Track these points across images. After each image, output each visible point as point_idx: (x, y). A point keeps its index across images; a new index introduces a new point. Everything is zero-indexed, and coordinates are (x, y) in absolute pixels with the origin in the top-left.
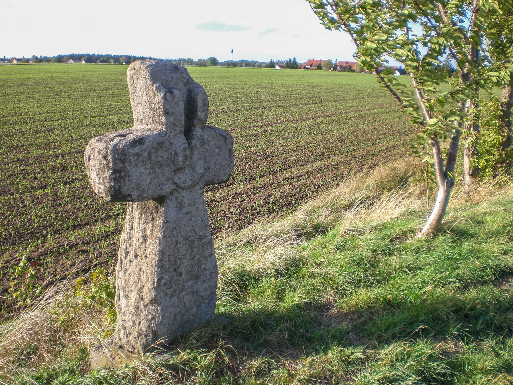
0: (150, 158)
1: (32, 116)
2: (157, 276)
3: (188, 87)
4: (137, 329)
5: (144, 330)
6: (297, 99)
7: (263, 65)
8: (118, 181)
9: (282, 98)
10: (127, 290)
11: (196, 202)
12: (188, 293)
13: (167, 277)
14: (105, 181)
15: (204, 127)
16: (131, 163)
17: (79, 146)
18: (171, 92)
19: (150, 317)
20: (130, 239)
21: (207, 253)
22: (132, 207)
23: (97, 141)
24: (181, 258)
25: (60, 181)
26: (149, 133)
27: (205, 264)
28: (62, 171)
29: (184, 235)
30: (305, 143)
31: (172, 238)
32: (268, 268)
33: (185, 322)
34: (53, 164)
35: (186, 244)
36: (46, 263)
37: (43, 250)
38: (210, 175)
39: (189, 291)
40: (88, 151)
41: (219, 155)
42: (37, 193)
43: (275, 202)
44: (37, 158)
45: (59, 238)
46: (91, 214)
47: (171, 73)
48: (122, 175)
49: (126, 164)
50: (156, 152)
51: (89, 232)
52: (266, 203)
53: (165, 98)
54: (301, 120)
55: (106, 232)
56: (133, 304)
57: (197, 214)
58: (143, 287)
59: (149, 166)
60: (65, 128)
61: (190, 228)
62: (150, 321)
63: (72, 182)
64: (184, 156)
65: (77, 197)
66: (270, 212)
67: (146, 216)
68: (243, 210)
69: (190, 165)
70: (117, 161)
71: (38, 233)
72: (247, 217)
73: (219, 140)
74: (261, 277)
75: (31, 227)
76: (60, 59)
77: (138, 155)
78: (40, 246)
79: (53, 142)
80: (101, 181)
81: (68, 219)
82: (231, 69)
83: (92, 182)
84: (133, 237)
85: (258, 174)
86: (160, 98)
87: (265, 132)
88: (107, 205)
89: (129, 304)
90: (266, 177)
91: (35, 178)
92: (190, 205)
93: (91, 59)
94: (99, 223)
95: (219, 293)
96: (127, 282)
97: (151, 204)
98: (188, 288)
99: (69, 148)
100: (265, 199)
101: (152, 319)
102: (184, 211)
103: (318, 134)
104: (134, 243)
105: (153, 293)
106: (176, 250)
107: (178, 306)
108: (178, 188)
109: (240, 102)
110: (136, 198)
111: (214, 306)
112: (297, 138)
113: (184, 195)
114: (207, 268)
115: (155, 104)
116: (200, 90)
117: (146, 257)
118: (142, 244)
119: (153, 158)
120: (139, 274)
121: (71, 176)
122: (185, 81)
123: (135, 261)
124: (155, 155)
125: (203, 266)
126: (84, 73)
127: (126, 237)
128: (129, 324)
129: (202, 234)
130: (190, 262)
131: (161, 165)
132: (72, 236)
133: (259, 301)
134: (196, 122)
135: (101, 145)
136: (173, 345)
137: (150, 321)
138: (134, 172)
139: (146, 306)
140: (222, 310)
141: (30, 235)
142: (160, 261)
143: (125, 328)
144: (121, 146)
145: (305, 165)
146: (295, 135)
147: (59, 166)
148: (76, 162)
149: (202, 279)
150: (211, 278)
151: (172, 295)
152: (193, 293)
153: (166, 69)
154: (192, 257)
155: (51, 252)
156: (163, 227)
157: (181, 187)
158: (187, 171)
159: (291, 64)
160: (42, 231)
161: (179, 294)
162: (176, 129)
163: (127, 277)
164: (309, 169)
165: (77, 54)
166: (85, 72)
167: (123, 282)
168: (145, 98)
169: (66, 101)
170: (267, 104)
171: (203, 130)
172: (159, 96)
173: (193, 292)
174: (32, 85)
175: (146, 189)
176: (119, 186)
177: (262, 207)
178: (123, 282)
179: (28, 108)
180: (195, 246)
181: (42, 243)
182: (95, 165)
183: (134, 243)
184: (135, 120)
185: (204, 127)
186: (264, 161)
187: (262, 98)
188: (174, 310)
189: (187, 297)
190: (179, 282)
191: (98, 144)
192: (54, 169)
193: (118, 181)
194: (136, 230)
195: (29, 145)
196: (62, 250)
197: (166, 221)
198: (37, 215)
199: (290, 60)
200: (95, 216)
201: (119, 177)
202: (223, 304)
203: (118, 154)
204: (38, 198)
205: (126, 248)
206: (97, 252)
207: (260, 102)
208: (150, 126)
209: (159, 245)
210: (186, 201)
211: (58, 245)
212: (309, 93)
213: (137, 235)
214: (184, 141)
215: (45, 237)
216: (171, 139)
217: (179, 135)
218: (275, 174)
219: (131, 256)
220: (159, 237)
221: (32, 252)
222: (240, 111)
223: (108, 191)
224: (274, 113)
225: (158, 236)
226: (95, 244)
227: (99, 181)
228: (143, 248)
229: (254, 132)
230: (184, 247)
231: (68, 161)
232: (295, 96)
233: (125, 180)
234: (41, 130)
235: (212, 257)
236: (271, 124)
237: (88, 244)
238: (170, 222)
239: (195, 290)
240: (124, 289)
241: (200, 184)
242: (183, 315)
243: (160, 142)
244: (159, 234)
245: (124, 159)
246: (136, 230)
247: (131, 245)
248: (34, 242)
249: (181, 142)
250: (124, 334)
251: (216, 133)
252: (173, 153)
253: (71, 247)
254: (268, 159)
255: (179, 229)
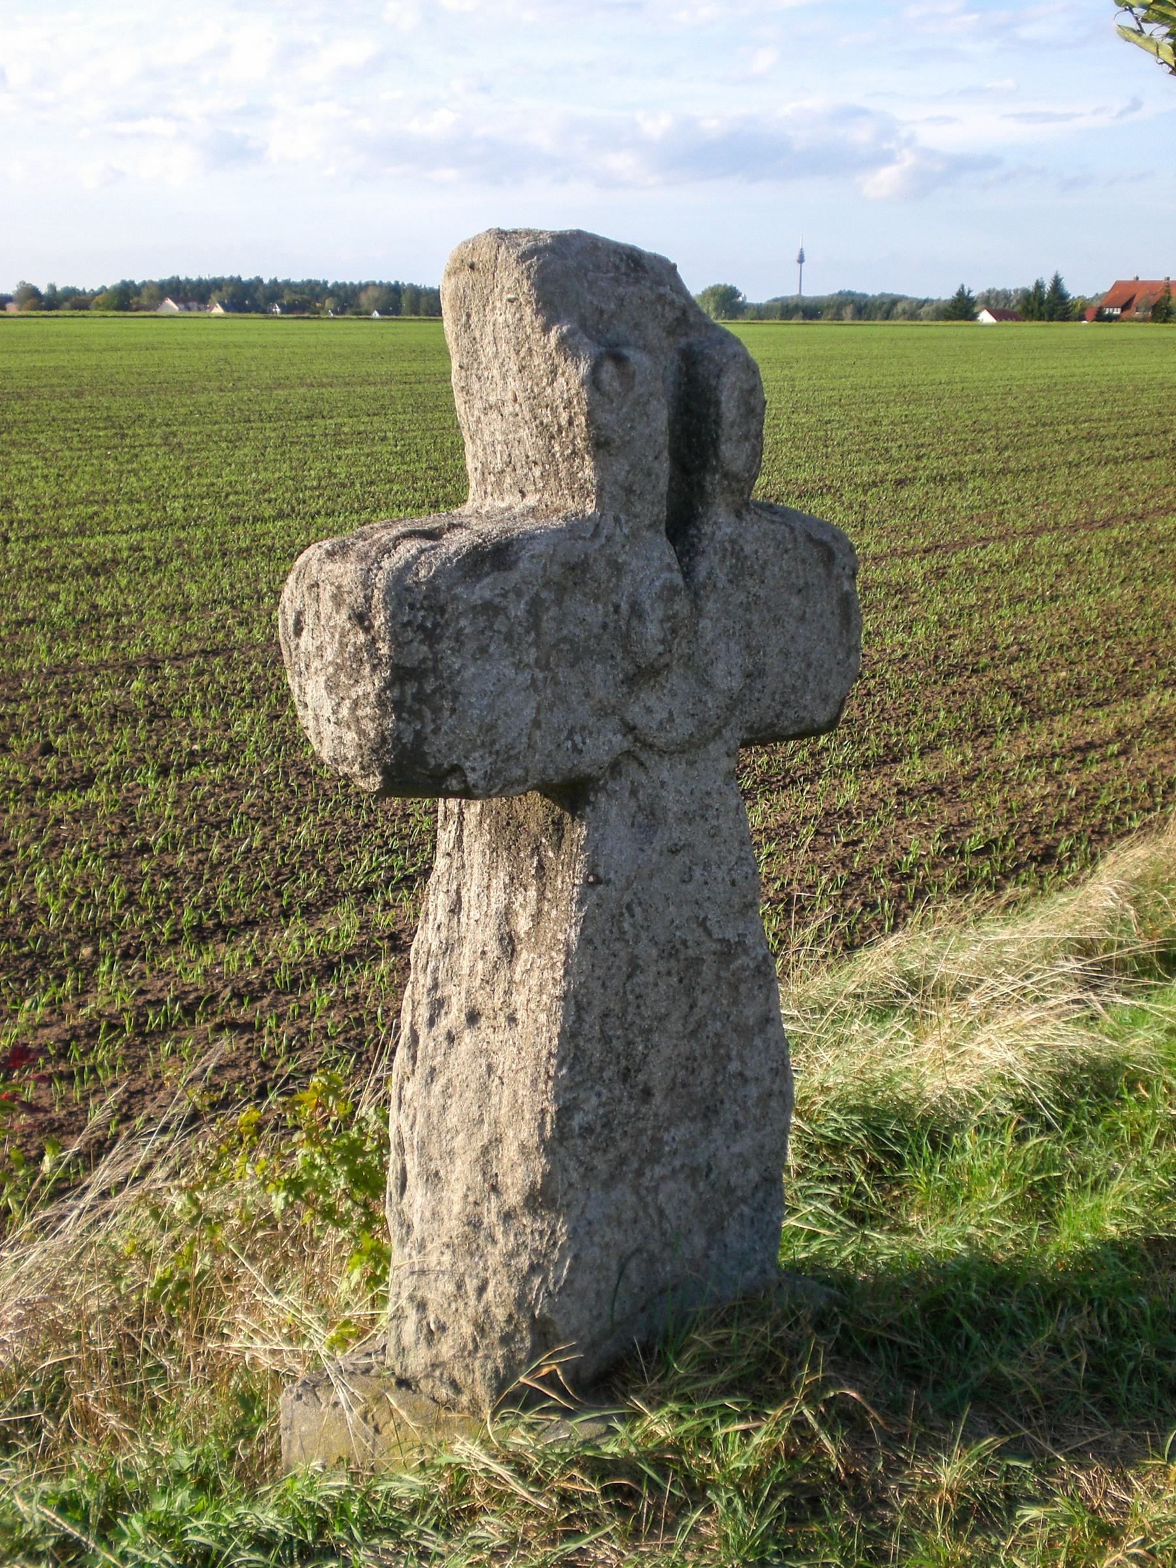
0: (535, 626)
1: (28, 515)
2: (556, 1097)
3: (683, 341)
4: (471, 1311)
5: (500, 1314)
6: (1072, 440)
7: (925, 309)
8: (411, 712)
9: (1005, 440)
10: (434, 1151)
11: (708, 807)
12: (674, 1171)
13: (594, 1101)
14: (360, 713)
15: (743, 507)
16: (462, 644)
17: (215, 630)
18: (619, 360)
19: (524, 1262)
20: (448, 948)
21: (751, 1013)
22: (461, 823)
23: (331, 554)
24: (650, 1031)
25: (142, 760)
26: (530, 525)
27: (741, 1057)
28: (150, 722)
29: (662, 939)
30: (1108, 615)
31: (618, 946)
32: (984, 1094)
33: (662, 1291)
34: (118, 695)
35: (669, 973)
36: (93, 1070)
37: (80, 1021)
38: (766, 701)
39: (677, 1163)
40: (292, 595)
41: (802, 619)
42: (57, 805)
43: (986, 850)
44: (52, 673)
45: (142, 976)
46: (266, 887)
47: (616, 280)
48: (428, 689)
49: (445, 645)
50: (559, 602)
51: (260, 953)
52: (950, 850)
53: (593, 381)
54: (1089, 524)
55: (323, 954)
56: (456, 1208)
57: (714, 856)
58: (498, 1141)
59: (531, 656)
60: (158, 562)
61: (687, 911)
62: (526, 1280)
63: (191, 765)
64: (669, 618)
65: (212, 819)
66: (963, 887)
67: (515, 860)
68: (858, 876)
69: (690, 657)
70: (410, 634)
71: (60, 956)
72: (873, 906)
73: (804, 561)
74: (957, 1127)
75: (32, 931)
76: (126, 298)
77: (489, 609)
78: (68, 1006)
79: (111, 615)
80: (345, 712)
81: (179, 902)
82: (796, 328)
83: (306, 719)
84: (461, 940)
85: (912, 738)
86: (575, 383)
87: (940, 573)
88: (326, 850)
89: (443, 1209)
90: (948, 752)
91: (48, 749)
92: (687, 817)
93: (246, 298)
94: (298, 923)
95: (792, 1185)
96: (435, 1119)
97: (534, 809)
98: (675, 1153)
99: (174, 638)
100: (945, 836)
101: (534, 1269)
102: (661, 840)
103: (1160, 580)
104: (465, 964)
105: (540, 1164)
106: (630, 997)
107: (635, 1221)
108: (640, 746)
109: (836, 459)
110: (482, 783)
111: (773, 1235)
112: (1073, 595)
113: (665, 776)
114: (748, 1073)
115: (554, 410)
116: (730, 351)
117: (512, 1019)
118: (495, 968)
119: (547, 625)
120: (484, 1087)
121: (186, 742)
122: (670, 315)
123: (468, 1039)
124: (553, 611)
125: (734, 1066)
126: (221, 353)
127: (435, 943)
128: (438, 1292)
129: (731, 935)
130: (684, 1047)
131: (577, 655)
132: (192, 968)
133: (951, 1225)
134: (713, 482)
135: (346, 572)
136: (603, 1382)
137: (526, 1280)
138: (474, 677)
139: (507, 1216)
140: (800, 1252)
141: (28, 963)
142: (570, 1036)
143: (422, 1306)
144: (422, 573)
145: (1107, 702)
146: (1065, 586)
147: (140, 704)
148: (204, 691)
149: (730, 1118)
150: (765, 1116)
151: (612, 1177)
152: (694, 1173)
153: (597, 268)
154: (691, 1027)
155: (111, 1027)
156: (581, 903)
157: (651, 746)
158: (676, 679)
159: (1041, 302)
160: (75, 946)
161: (639, 1173)
162: (638, 508)
163: (434, 1102)
164: (1128, 720)
165: (194, 278)
166: (226, 347)
167: (420, 1119)
168: (513, 385)
169: (155, 459)
170: (947, 465)
171: (739, 515)
172: (572, 377)
173: (695, 1170)
174: (20, 397)
175: (522, 746)
176: (417, 734)
177: (934, 866)
178: (420, 1119)
179: (10, 486)
180: (704, 984)
181: (76, 992)
182: (320, 648)
183: (465, 964)
184: (473, 478)
185: (743, 507)
186: (938, 688)
187: (927, 440)
188: (619, 1237)
189: (671, 1185)
190: (640, 1124)
191: (335, 568)
192: (117, 715)
193: (411, 712)
194: (475, 914)
195: (19, 624)
196: (154, 1020)
197: (594, 881)
198: (56, 886)
199: (1039, 286)
200: (279, 894)
201: (415, 697)
202: (808, 1227)
203: (412, 606)
204: (59, 821)
205: (435, 986)
206: (292, 1031)
207: (918, 458)
208: (532, 500)
209: (566, 973)
210: (671, 801)
211: (141, 1000)
212: (1122, 416)
213: (479, 934)
214: (667, 560)
215: (88, 969)
216: (618, 548)
217: (646, 534)
218: (983, 740)
219: (452, 1018)
220: (567, 944)
221: (36, 1029)
222: (837, 494)
223: (374, 751)
224: (975, 499)
225: (561, 937)
226: (284, 999)
227: (335, 712)
228: (503, 986)
229: (895, 575)
230: (662, 987)
231: (172, 685)
232: (1062, 429)
233: (437, 710)
234: (64, 567)
235: (771, 1030)
236: (964, 543)
237: (253, 1000)
238: (608, 882)
239: (701, 1160)
240: (423, 1145)
241: (726, 733)
242: (652, 1260)
243: (573, 563)
244: (564, 928)
245: (436, 625)
246: (475, 914)
247: (452, 973)
248: (45, 990)
249: (657, 564)
250: (419, 1330)
251: (792, 530)
252: (624, 607)
253: (189, 1011)
254: (953, 681)
255: (645, 911)
